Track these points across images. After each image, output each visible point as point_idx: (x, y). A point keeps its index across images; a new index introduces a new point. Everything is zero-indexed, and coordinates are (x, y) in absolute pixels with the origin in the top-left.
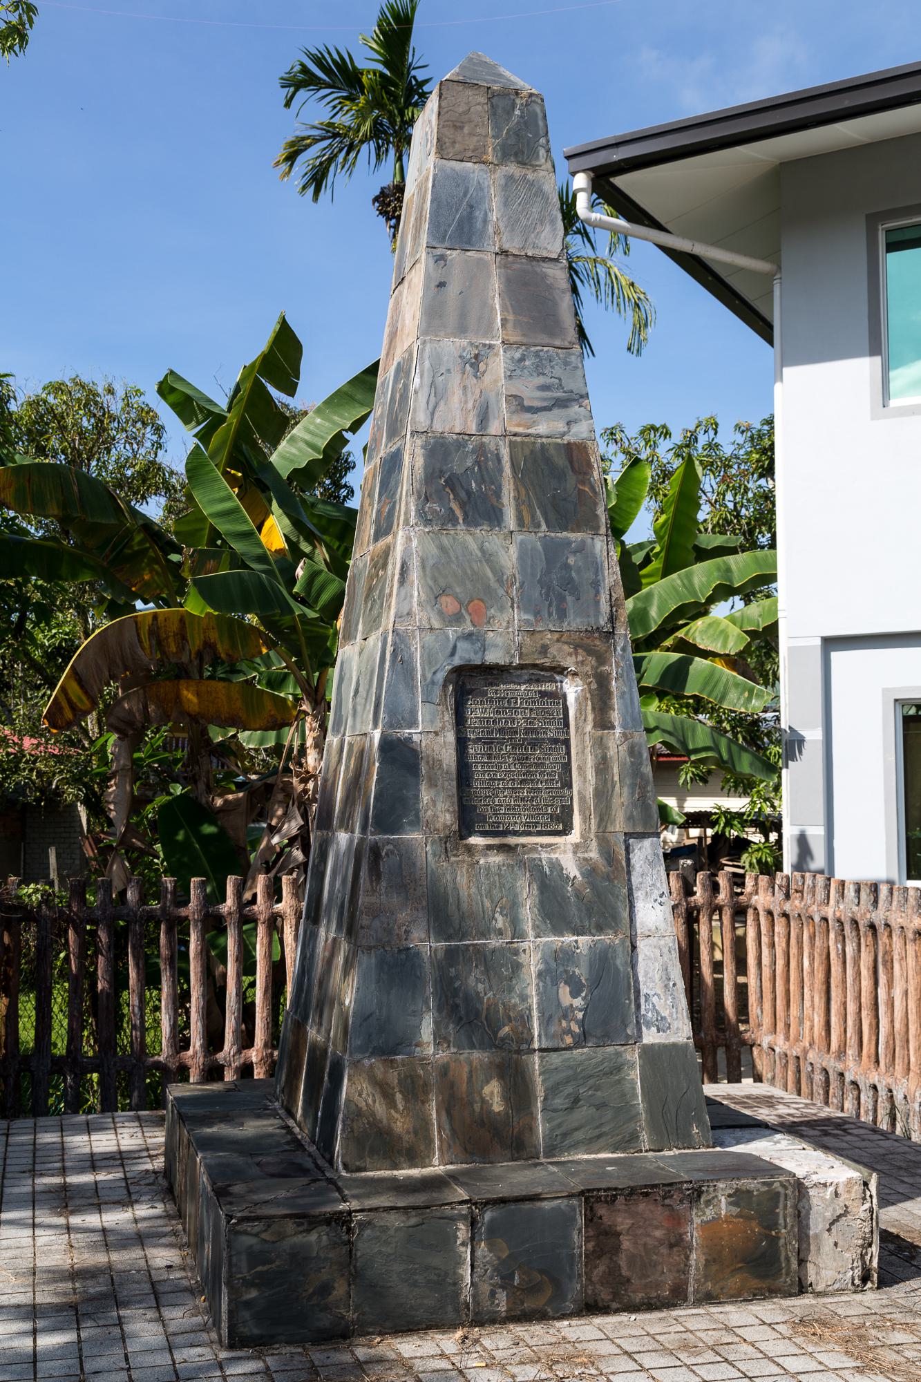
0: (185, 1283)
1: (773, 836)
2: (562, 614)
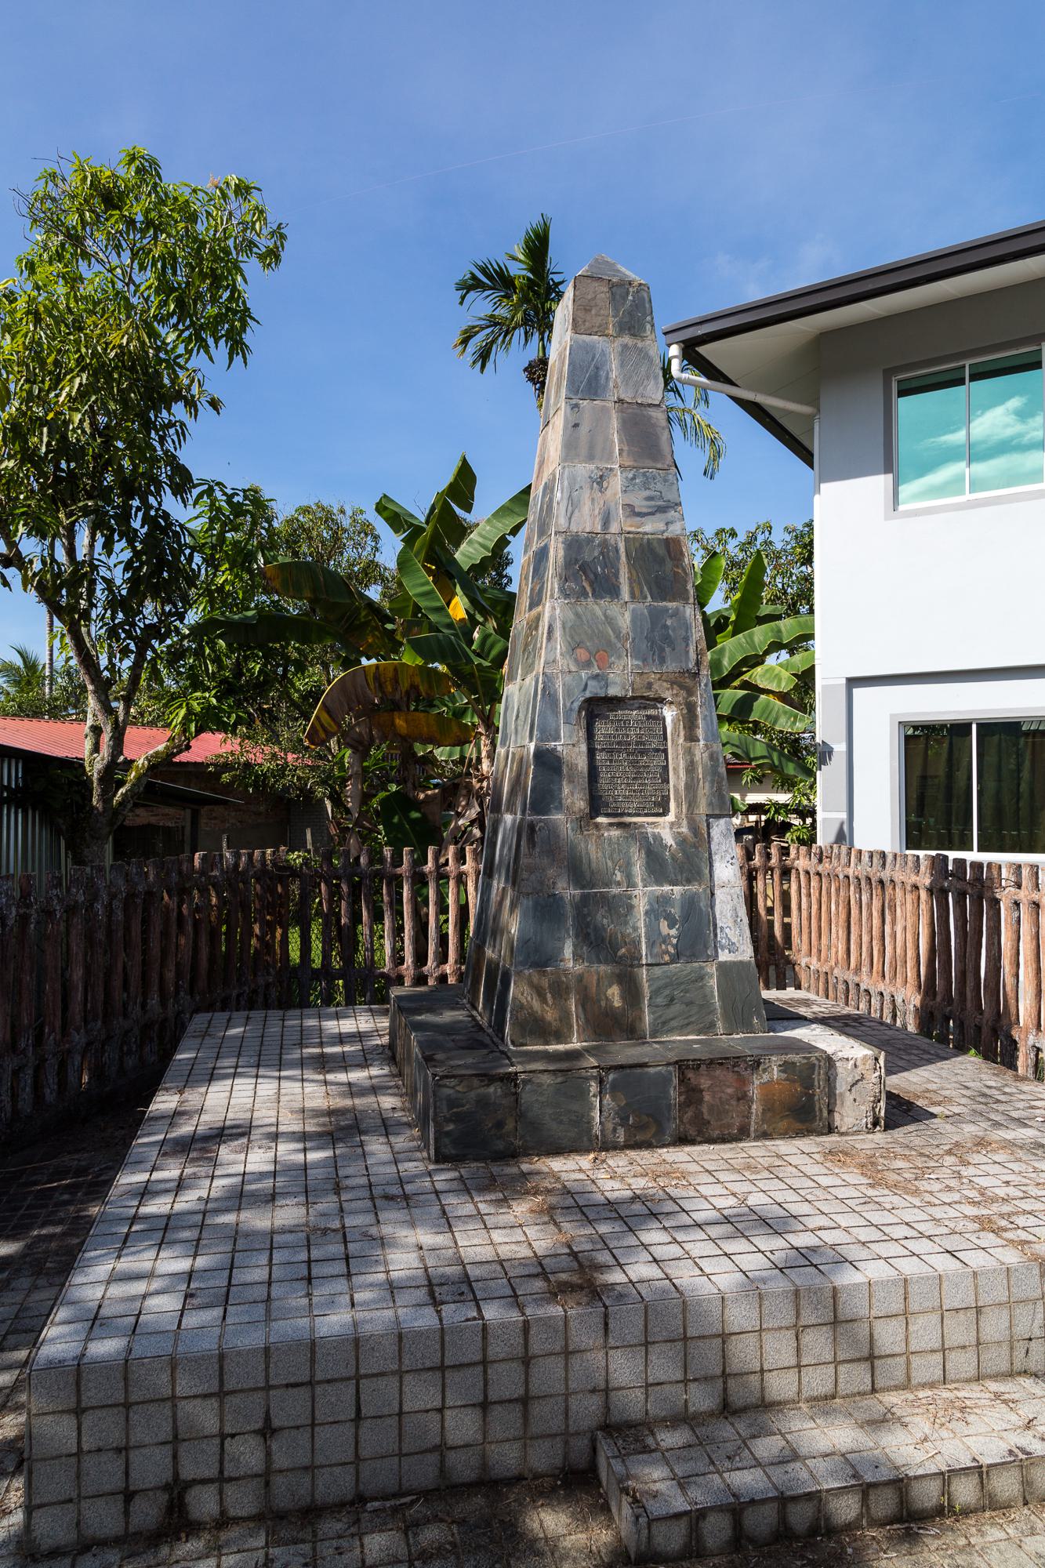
0: (405, 1119)
1: (809, 821)
2: (662, 661)
